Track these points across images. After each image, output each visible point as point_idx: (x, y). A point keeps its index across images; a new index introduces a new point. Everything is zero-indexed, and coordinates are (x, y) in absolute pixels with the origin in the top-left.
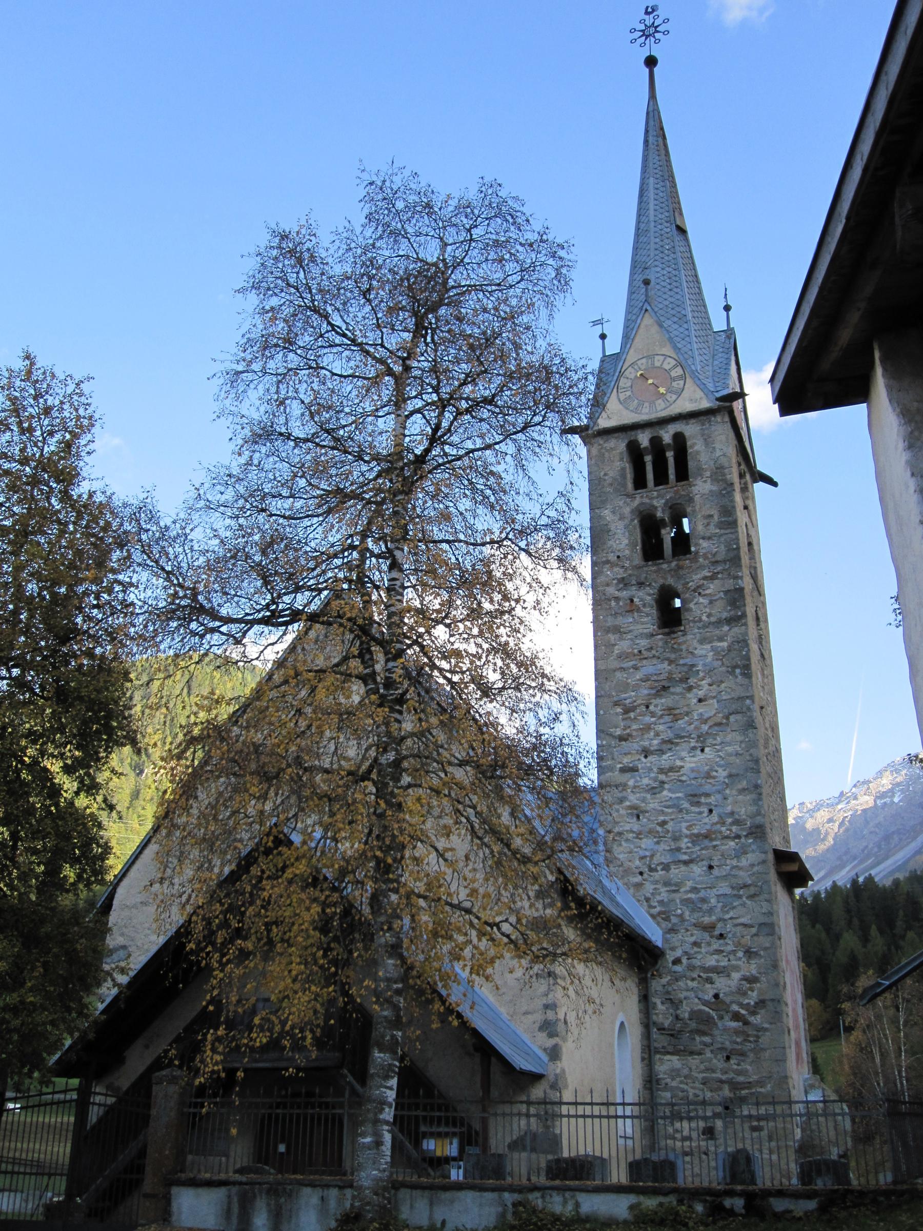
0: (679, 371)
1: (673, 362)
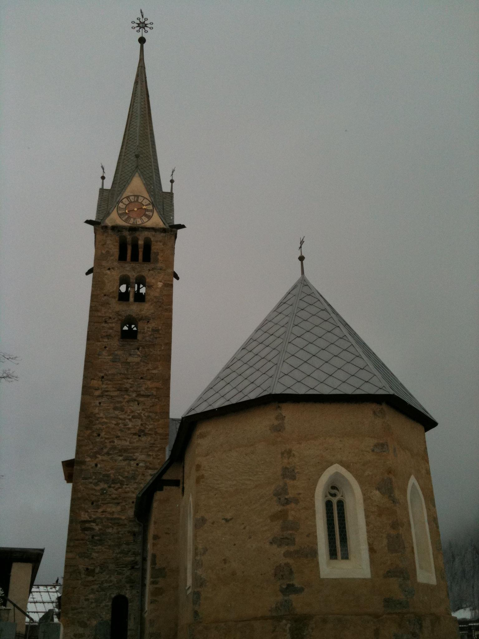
0: (150, 207)
1: (148, 202)
